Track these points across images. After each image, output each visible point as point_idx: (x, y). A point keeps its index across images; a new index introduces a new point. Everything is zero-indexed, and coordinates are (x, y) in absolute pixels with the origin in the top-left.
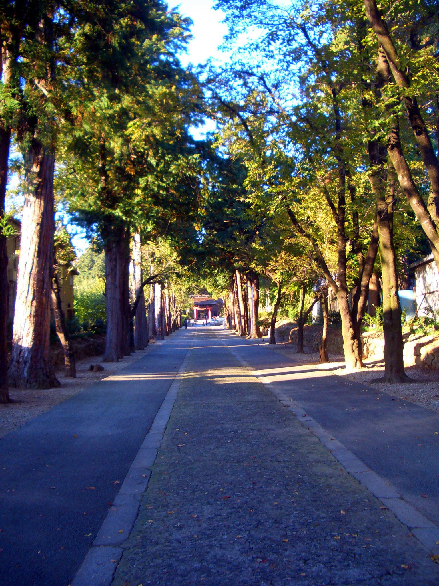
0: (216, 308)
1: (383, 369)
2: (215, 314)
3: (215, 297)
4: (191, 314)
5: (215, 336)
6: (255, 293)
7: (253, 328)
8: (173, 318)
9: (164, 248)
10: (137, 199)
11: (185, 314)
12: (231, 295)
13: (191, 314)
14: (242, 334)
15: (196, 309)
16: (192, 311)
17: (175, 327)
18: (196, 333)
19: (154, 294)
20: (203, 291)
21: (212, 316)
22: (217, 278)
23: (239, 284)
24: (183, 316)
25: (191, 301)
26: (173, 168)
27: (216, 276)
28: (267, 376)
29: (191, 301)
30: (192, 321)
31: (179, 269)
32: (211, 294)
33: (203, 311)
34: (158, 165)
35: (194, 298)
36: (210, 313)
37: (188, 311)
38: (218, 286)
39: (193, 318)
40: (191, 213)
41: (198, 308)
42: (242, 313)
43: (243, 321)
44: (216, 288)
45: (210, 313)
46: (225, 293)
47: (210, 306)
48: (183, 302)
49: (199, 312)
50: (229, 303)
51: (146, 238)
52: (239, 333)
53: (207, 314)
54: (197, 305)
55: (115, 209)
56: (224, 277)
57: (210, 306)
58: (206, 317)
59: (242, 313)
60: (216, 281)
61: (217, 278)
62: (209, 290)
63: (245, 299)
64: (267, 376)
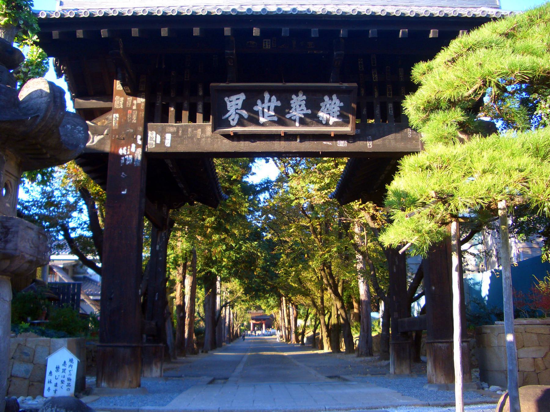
0: (269, 322)
1: (52, 257)
2: (268, 326)
3: (268, 313)
4: (248, 327)
5: (267, 342)
6: (295, 312)
7: (293, 336)
8: (235, 329)
9: (235, 284)
10: (224, 263)
11: (243, 326)
12: (280, 311)
13: (248, 327)
14: (286, 341)
15: (252, 322)
16: (249, 324)
17: (236, 336)
18: (252, 341)
19: (226, 313)
20: (259, 308)
21: (266, 328)
22: (269, 300)
23: (284, 304)
24: (241, 328)
25: (249, 316)
26: (244, 248)
27: (268, 298)
28: (286, 354)
29: (249, 316)
30: (249, 332)
31: (244, 298)
32: (265, 311)
33: (258, 324)
34: (236, 246)
35: (250, 313)
36: (264, 326)
37: (245, 323)
38: (269, 306)
39: (250, 330)
40: (252, 268)
41: (254, 322)
42: (287, 326)
43: (287, 331)
44: (267, 306)
45: (264, 326)
46: (275, 310)
47: (264, 320)
48: (243, 317)
49: (254, 325)
50: (279, 317)
51: (225, 280)
52: (285, 341)
53: (262, 327)
54: (253, 319)
55: (212, 268)
56: (274, 299)
57: (264, 320)
58: (260, 328)
59: (287, 326)
60: (268, 302)
61: (269, 300)
62: (263, 307)
63: (288, 315)
64: (286, 354)
